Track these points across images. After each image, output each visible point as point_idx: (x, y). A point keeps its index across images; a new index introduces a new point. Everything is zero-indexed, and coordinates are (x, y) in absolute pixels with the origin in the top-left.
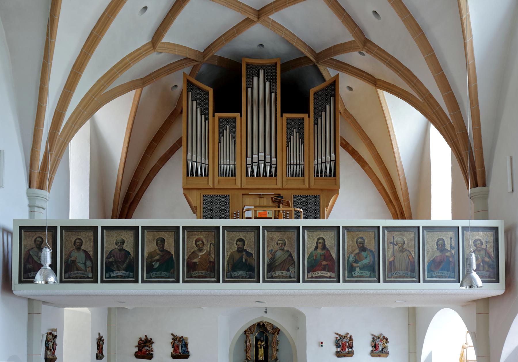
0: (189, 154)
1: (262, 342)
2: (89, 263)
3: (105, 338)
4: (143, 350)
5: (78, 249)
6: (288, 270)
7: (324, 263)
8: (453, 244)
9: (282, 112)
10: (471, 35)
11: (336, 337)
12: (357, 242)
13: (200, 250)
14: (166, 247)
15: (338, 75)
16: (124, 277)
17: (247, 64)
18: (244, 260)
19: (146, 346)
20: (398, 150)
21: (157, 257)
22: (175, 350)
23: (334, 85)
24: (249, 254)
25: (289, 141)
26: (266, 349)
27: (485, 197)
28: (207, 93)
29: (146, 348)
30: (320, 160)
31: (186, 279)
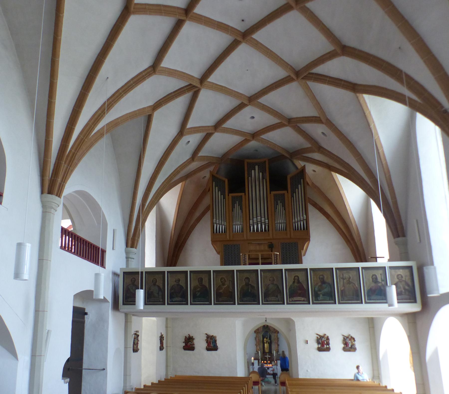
0: (215, 220)
1: (267, 338)
2: (160, 293)
3: (164, 336)
4: (188, 344)
5: (155, 285)
6: (277, 296)
7: (299, 292)
8: (383, 278)
9: (271, 191)
10: (382, 147)
11: (317, 337)
12: (319, 278)
13: (224, 284)
14: (203, 283)
15: (305, 165)
16: (180, 301)
17: (248, 163)
18: (250, 291)
19: (190, 341)
20: (350, 207)
21: (198, 289)
22: (208, 345)
23: (302, 171)
24: (253, 287)
25: (276, 208)
26: (270, 344)
27: (405, 244)
28: (224, 181)
29: (190, 343)
30: (296, 219)
31: (216, 302)
